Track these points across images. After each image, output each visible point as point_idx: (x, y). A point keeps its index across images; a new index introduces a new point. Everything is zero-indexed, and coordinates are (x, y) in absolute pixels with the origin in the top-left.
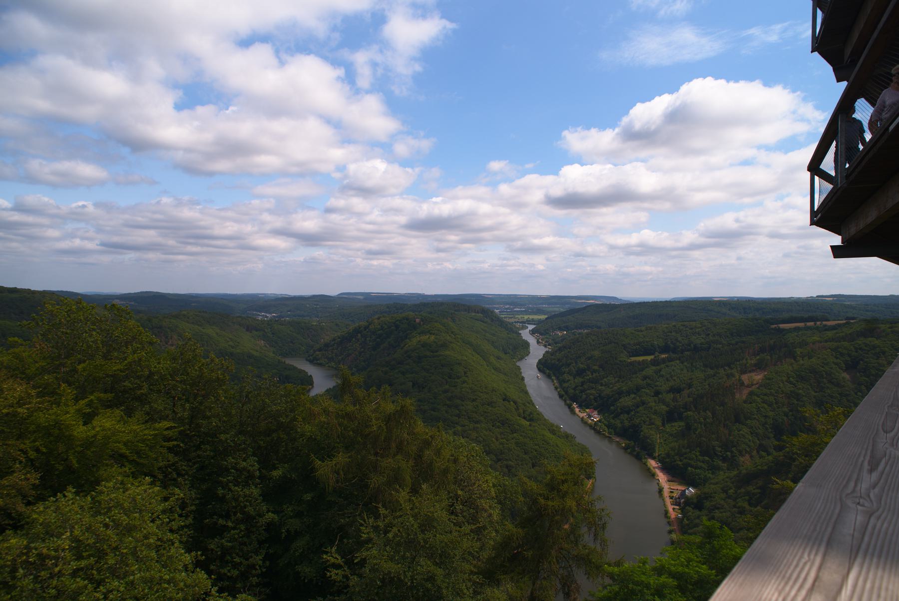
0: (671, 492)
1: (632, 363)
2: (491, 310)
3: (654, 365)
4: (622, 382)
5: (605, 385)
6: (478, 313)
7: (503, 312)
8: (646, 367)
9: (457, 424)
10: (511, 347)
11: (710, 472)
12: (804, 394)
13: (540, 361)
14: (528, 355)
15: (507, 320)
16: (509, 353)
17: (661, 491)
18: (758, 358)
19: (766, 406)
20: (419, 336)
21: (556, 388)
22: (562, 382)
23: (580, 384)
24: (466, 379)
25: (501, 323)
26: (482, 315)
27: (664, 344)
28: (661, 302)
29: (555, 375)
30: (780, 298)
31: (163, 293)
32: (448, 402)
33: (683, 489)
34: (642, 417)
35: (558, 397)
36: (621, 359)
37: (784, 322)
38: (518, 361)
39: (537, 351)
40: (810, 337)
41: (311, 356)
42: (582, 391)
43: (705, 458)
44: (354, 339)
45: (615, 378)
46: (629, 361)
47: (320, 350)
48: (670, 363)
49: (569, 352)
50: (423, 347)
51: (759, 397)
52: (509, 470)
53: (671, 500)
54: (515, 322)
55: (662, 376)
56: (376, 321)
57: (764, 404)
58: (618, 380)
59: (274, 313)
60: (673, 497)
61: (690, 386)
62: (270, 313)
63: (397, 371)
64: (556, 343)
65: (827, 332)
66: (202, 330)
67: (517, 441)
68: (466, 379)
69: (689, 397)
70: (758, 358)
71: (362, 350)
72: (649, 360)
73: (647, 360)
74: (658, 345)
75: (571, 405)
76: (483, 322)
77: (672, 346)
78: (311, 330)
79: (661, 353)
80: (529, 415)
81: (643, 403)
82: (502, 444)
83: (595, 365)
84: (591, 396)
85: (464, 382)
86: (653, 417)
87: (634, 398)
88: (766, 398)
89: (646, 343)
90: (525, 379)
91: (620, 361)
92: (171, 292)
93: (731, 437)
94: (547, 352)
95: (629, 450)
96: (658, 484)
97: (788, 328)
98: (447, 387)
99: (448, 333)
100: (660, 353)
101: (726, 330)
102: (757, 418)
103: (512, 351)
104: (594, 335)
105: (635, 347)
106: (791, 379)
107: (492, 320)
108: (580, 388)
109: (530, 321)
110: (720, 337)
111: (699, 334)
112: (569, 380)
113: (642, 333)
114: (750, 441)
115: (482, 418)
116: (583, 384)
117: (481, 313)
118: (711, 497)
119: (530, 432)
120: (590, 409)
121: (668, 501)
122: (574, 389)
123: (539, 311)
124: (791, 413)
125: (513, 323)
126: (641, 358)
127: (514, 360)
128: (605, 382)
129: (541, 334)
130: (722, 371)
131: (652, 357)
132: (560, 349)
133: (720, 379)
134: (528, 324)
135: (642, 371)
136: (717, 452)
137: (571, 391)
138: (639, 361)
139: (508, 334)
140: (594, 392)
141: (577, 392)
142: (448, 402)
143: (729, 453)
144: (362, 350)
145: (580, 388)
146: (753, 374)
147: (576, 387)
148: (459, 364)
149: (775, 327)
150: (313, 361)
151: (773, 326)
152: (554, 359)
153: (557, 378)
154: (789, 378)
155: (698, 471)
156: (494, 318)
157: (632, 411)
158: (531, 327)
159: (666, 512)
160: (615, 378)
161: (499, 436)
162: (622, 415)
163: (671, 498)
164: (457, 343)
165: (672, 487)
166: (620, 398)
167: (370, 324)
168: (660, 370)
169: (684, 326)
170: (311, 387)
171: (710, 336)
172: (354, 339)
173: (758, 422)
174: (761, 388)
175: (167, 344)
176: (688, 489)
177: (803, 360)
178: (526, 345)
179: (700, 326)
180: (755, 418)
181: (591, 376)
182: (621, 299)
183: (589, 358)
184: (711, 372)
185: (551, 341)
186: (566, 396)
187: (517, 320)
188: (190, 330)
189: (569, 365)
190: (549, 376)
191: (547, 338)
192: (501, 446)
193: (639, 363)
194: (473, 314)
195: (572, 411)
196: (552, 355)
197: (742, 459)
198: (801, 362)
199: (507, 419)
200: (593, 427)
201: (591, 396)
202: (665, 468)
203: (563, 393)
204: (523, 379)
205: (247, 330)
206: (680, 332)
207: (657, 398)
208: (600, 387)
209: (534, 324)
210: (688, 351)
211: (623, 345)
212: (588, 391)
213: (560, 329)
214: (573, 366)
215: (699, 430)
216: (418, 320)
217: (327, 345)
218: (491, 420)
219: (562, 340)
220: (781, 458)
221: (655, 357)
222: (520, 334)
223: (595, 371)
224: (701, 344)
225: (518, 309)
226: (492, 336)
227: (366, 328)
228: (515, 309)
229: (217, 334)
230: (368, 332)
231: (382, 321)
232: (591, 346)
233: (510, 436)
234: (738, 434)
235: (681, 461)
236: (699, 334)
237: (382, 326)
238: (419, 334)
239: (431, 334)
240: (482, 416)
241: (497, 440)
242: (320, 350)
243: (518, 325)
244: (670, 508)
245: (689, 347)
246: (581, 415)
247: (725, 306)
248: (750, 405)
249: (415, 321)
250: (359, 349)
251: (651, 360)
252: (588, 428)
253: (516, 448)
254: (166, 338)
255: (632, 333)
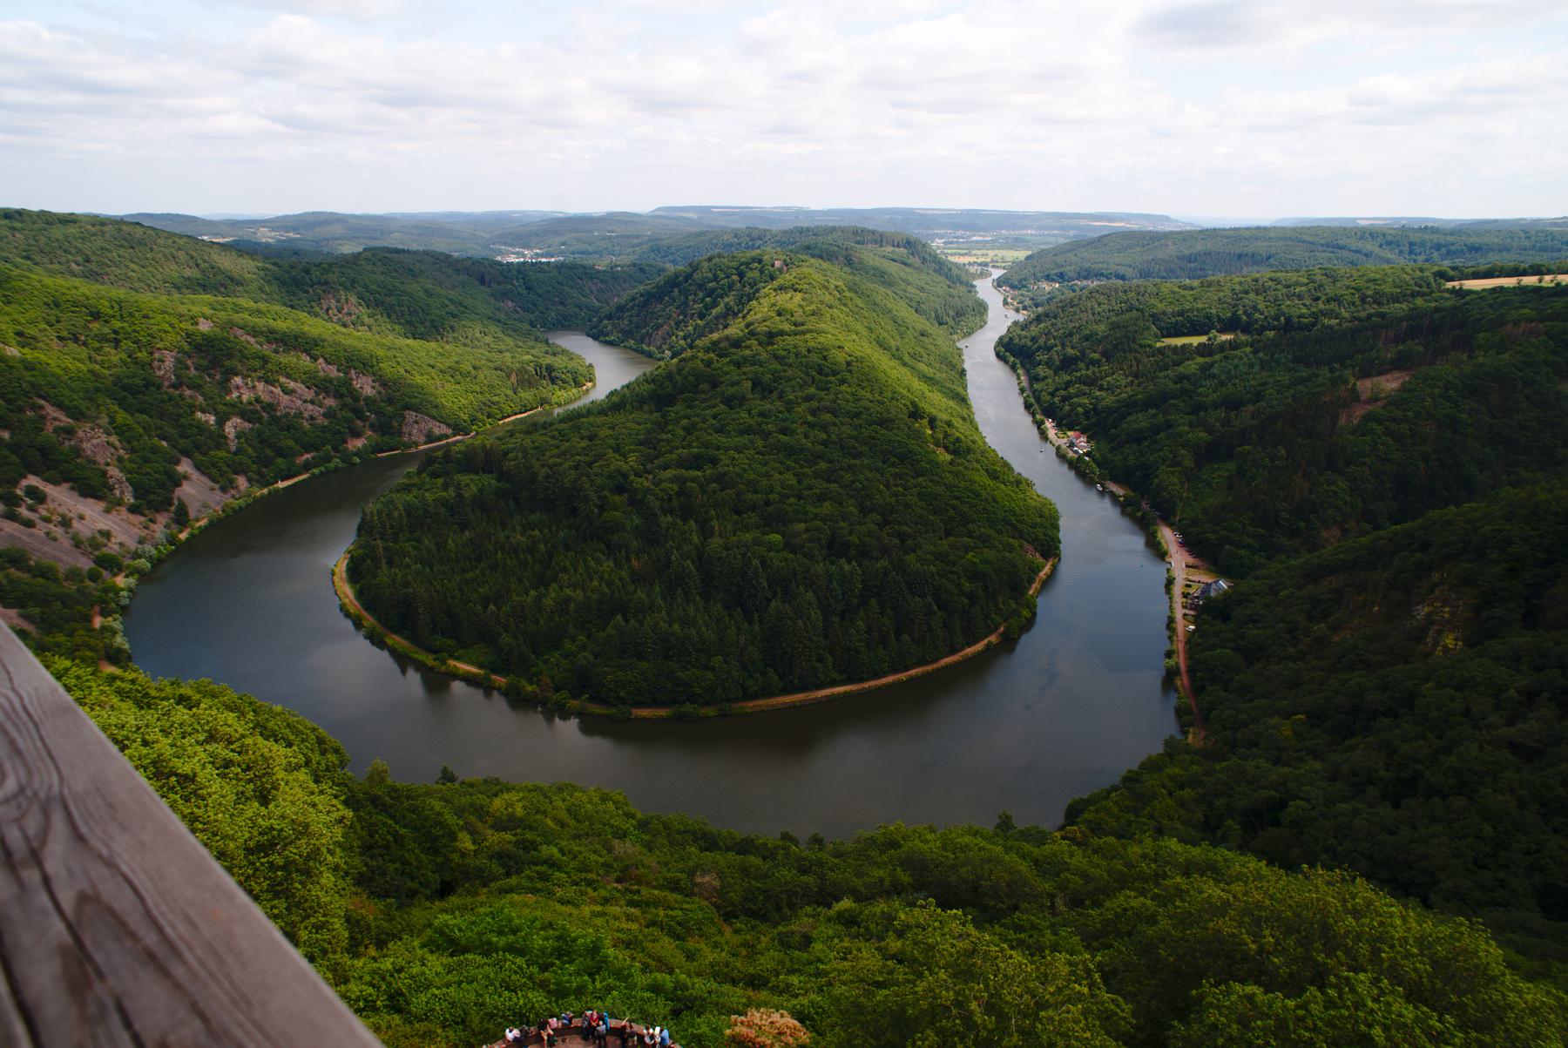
0: (1189, 586)
1: (1161, 351)
2: (923, 242)
3: (1203, 356)
4: (1139, 385)
5: (1107, 390)
6: (898, 246)
7: (951, 243)
8: (1188, 359)
9: (820, 457)
10: (951, 313)
11: (1263, 554)
12: (1470, 421)
13: (1001, 339)
14: (982, 327)
15: (951, 259)
16: (946, 323)
17: (1170, 583)
18: (1401, 347)
19: (1390, 441)
20: (774, 294)
21: (1022, 391)
22: (1033, 379)
23: (1064, 386)
24: (848, 375)
25: (941, 267)
26: (905, 251)
27: (1229, 315)
28: (1248, 229)
29: (1023, 366)
30: (1495, 221)
31: (484, 215)
32: (810, 418)
33: (1210, 581)
34: (1161, 450)
35: (1021, 408)
36: (1143, 342)
37: (1477, 275)
38: (963, 338)
39: (1001, 319)
40: (1516, 308)
41: (595, 328)
42: (1064, 399)
43: (1259, 530)
44: (667, 298)
45: (1127, 376)
46: (1159, 345)
47: (610, 317)
48: (1233, 352)
49: (1052, 324)
50: (779, 314)
51: (1381, 424)
52: (902, 541)
53: (1184, 600)
54: (970, 264)
55: (1214, 376)
56: (705, 264)
57: (1388, 438)
58: (1132, 382)
59: (535, 248)
60: (1189, 594)
61: (1258, 397)
62: (528, 248)
63: (728, 359)
64: (1037, 306)
65: (1555, 299)
66: (399, 286)
67: (924, 490)
68: (848, 375)
69: (1253, 418)
70: (1401, 347)
71: (681, 317)
72: (1195, 345)
73: (1191, 345)
74: (1218, 316)
75: (1043, 423)
76: (905, 264)
77: (1244, 318)
78: (595, 280)
79: (1221, 331)
80: (954, 444)
81: (1169, 425)
82: (895, 495)
83: (1094, 352)
84: (1080, 409)
85: (843, 382)
86: (1182, 452)
87: (1154, 416)
88: (1394, 426)
89: (1195, 313)
90: (968, 373)
91: (1142, 346)
92: (357, 212)
93: (1313, 496)
94: (1016, 323)
95: (1129, 509)
96: (1168, 570)
97: (1479, 288)
98: (812, 390)
99: (827, 289)
100: (1219, 331)
101: (1353, 291)
102: (1369, 463)
103: (954, 319)
104: (1102, 293)
105: (1173, 320)
106: (1452, 392)
107: (924, 261)
108: (1063, 393)
109: (997, 262)
110: (1339, 305)
111: (1300, 297)
112: (1046, 378)
113: (1191, 293)
114: (1346, 503)
115: (865, 448)
116: (1068, 384)
117: (905, 247)
118: (1248, 601)
119: (948, 475)
120: (1075, 430)
121: (1178, 600)
122: (1052, 394)
123: (1016, 243)
124: (1435, 456)
125: (964, 265)
126: (1179, 342)
127: (955, 336)
128: (1109, 382)
129: (1013, 287)
130: (1324, 371)
131: (1203, 339)
132: (1038, 319)
133: (1317, 387)
134: (993, 267)
135: (1179, 365)
136: (1281, 522)
137: (1045, 397)
138: (1176, 346)
139: (949, 287)
140: (1086, 401)
141: (1056, 400)
142: (810, 418)
143: (1302, 524)
144: (681, 317)
145: (1063, 393)
146: (1382, 379)
147: (1057, 389)
148: (840, 347)
149: (1454, 287)
150: (598, 336)
151: (1450, 285)
152: (1026, 337)
153: (1028, 372)
154: (1447, 390)
155: (1242, 552)
156: (927, 257)
157: (1146, 438)
158: (997, 273)
159: (1171, 620)
160: (1127, 376)
161: (892, 482)
162: (1127, 446)
163: (1185, 595)
164: (842, 307)
165: (1190, 578)
166: (1130, 414)
167: (695, 271)
168: (1212, 365)
169: (1275, 280)
170: (590, 384)
171: (1320, 302)
172: (667, 298)
173: (1368, 471)
174: (1389, 408)
175: (340, 312)
176: (1216, 582)
177: (1485, 356)
178: (981, 309)
179: (1306, 281)
180: (1364, 463)
181: (1084, 372)
182: (1176, 221)
183: (1087, 338)
184: (1304, 373)
185: (1028, 302)
186: (1036, 406)
187: (972, 259)
188: (378, 286)
189: (1049, 349)
190: (1013, 368)
191: (1022, 295)
192: (894, 499)
193: (1175, 349)
194: (890, 249)
195: (1043, 435)
196: (1023, 330)
197: (1324, 534)
198: (1481, 360)
199: (910, 452)
200: (1076, 466)
201: (1080, 409)
202: (1188, 544)
203: (1032, 400)
204: (963, 373)
205: (483, 282)
206: (1265, 292)
207: (1195, 417)
208: (1098, 393)
209: (1004, 268)
210: (1273, 329)
211: (1153, 316)
212: (1076, 400)
213: (1048, 278)
214: (1056, 351)
215: (1259, 480)
216: (778, 264)
217: (621, 308)
218: (881, 452)
219: (1050, 300)
220: (1382, 542)
221: (1209, 339)
222: (974, 286)
223: (1093, 363)
224: (1300, 317)
225: (979, 238)
226: (918, 292)
227: (688, 277)
228: (974, 238)
229: (426, 291)
230: (690, 285)
231: (715, 265)
232: (1093, 314)
233: (912, 481)
234: (1327, 491)
235: (1214, 532)
236: (1300, 297)
237: (714, 274)
238: (775, 290)
239: (795, 290)
240: (866, 444)
241: (887, 486)
242: (610, 317)
243: (972, 270)
244: (1179, 613)
245: (1276, 323)
246: (1063, 442)
247: (1373, 237)
248: (1360, 438)
249: (773, 265)
250: (674, 315)
251: (1199, 345)
252: (1066, 466)
253: (919, 503)
254: (338, 301)
255: (1173, 293)
